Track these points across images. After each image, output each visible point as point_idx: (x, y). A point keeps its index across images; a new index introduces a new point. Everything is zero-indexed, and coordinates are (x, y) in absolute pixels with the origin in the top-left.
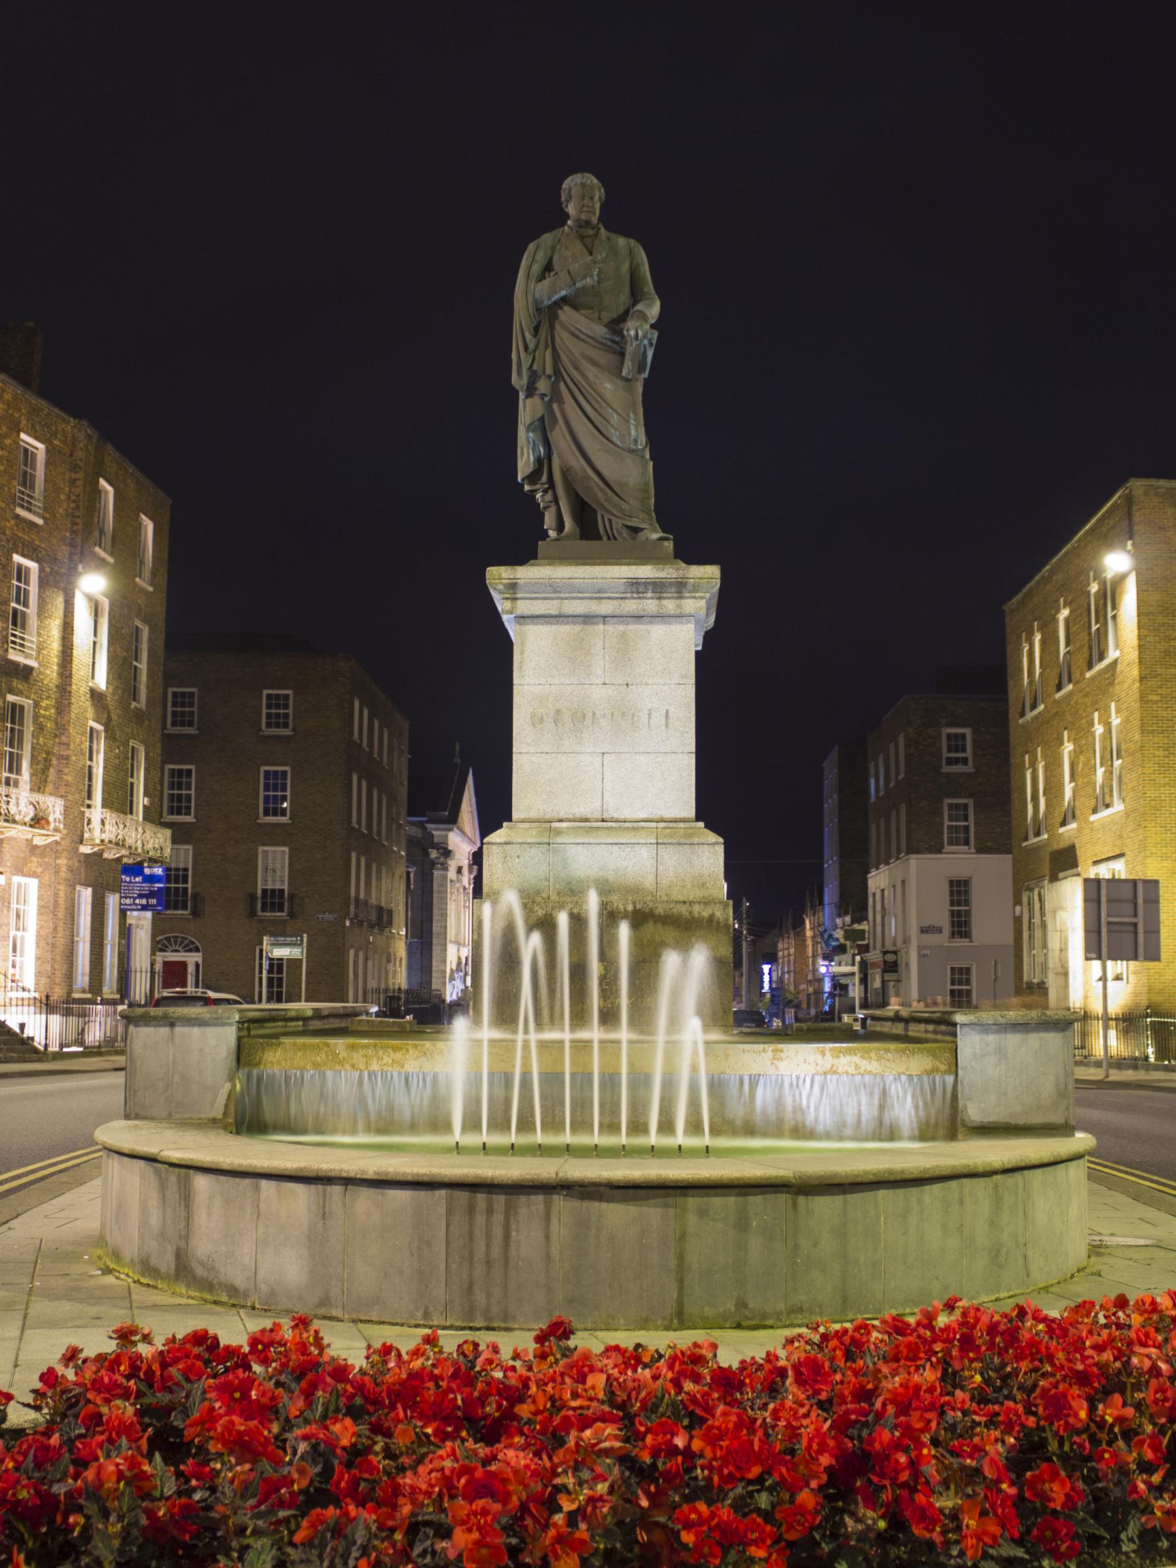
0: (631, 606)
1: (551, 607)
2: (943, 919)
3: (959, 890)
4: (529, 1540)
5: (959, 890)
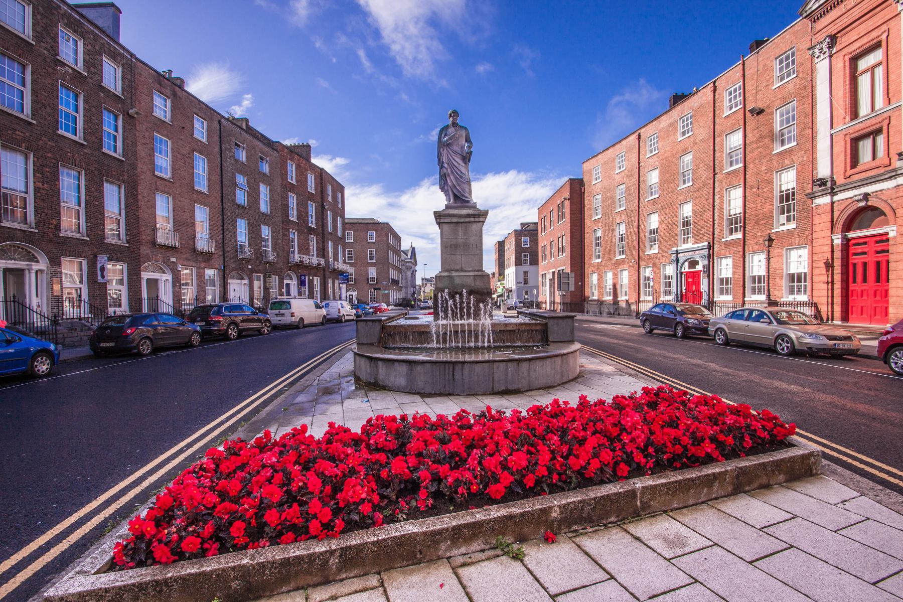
0: (467, 220)
1: (449, 220)
2: (522, 281)
3: (526, 273)
4: (571, 535)
5: (526, 273)
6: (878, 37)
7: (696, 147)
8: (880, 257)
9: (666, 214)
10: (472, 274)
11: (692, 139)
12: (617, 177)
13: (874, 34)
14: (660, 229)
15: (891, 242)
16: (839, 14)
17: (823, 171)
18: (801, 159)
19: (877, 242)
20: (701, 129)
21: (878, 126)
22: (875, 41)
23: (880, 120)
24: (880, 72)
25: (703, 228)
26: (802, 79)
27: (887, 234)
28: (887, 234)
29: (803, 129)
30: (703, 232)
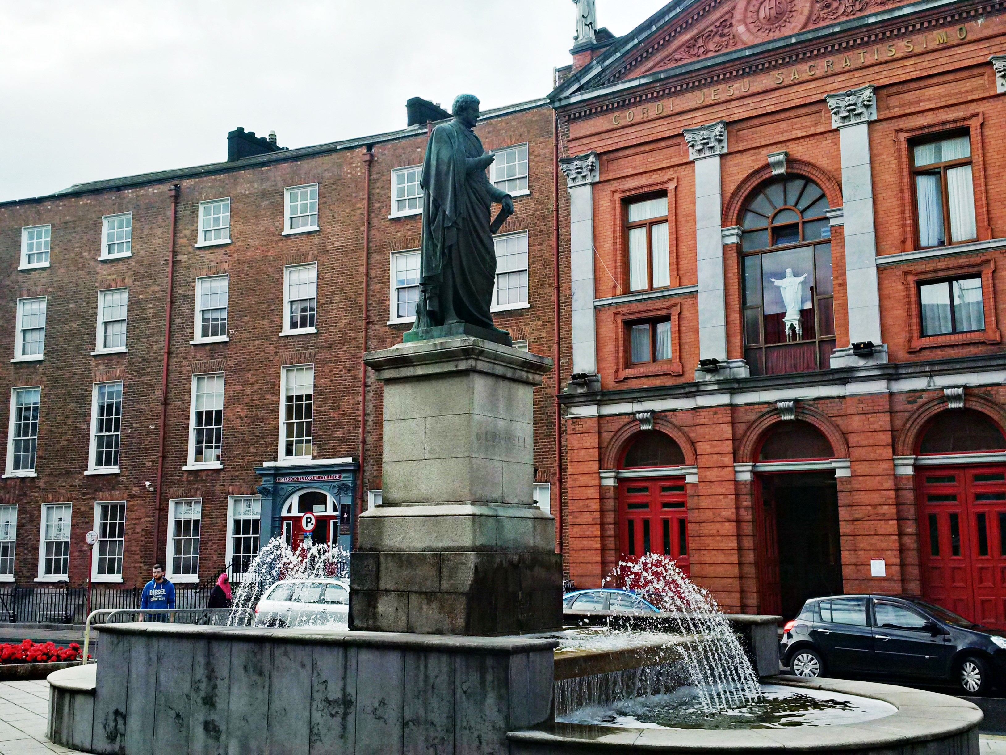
6: (663, 183)
7: (324, 259)
8: (673, 514)
9: (246, 383)
10: (468, 509)
11: (316, 240)
12: (103, 271)
13: (657, 178)
14: (230, 414)
15: (689, 492)
16: (606, 127)
17: (584, 361)
18: (536, 333)
19: (664, 489)
20: (338, 227)
21: (664, 312)
22: (658, 187)
23: (667, 304)
24: (661, 233)
25: (339, 426)
26: (538, 202)
27: (683, 477)
28: (683, 477)
29: (541, 285)
30: (339, 434)
